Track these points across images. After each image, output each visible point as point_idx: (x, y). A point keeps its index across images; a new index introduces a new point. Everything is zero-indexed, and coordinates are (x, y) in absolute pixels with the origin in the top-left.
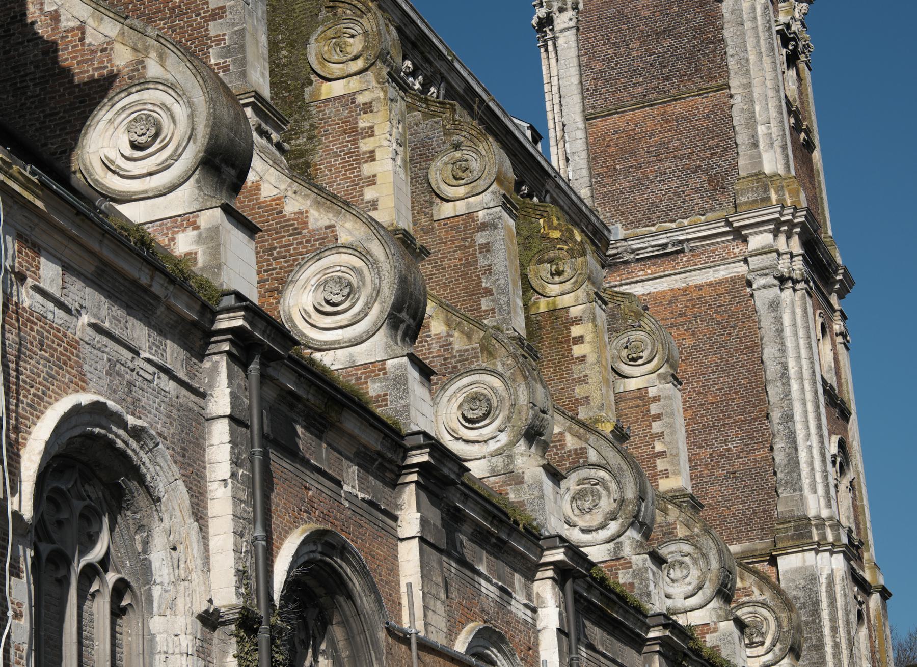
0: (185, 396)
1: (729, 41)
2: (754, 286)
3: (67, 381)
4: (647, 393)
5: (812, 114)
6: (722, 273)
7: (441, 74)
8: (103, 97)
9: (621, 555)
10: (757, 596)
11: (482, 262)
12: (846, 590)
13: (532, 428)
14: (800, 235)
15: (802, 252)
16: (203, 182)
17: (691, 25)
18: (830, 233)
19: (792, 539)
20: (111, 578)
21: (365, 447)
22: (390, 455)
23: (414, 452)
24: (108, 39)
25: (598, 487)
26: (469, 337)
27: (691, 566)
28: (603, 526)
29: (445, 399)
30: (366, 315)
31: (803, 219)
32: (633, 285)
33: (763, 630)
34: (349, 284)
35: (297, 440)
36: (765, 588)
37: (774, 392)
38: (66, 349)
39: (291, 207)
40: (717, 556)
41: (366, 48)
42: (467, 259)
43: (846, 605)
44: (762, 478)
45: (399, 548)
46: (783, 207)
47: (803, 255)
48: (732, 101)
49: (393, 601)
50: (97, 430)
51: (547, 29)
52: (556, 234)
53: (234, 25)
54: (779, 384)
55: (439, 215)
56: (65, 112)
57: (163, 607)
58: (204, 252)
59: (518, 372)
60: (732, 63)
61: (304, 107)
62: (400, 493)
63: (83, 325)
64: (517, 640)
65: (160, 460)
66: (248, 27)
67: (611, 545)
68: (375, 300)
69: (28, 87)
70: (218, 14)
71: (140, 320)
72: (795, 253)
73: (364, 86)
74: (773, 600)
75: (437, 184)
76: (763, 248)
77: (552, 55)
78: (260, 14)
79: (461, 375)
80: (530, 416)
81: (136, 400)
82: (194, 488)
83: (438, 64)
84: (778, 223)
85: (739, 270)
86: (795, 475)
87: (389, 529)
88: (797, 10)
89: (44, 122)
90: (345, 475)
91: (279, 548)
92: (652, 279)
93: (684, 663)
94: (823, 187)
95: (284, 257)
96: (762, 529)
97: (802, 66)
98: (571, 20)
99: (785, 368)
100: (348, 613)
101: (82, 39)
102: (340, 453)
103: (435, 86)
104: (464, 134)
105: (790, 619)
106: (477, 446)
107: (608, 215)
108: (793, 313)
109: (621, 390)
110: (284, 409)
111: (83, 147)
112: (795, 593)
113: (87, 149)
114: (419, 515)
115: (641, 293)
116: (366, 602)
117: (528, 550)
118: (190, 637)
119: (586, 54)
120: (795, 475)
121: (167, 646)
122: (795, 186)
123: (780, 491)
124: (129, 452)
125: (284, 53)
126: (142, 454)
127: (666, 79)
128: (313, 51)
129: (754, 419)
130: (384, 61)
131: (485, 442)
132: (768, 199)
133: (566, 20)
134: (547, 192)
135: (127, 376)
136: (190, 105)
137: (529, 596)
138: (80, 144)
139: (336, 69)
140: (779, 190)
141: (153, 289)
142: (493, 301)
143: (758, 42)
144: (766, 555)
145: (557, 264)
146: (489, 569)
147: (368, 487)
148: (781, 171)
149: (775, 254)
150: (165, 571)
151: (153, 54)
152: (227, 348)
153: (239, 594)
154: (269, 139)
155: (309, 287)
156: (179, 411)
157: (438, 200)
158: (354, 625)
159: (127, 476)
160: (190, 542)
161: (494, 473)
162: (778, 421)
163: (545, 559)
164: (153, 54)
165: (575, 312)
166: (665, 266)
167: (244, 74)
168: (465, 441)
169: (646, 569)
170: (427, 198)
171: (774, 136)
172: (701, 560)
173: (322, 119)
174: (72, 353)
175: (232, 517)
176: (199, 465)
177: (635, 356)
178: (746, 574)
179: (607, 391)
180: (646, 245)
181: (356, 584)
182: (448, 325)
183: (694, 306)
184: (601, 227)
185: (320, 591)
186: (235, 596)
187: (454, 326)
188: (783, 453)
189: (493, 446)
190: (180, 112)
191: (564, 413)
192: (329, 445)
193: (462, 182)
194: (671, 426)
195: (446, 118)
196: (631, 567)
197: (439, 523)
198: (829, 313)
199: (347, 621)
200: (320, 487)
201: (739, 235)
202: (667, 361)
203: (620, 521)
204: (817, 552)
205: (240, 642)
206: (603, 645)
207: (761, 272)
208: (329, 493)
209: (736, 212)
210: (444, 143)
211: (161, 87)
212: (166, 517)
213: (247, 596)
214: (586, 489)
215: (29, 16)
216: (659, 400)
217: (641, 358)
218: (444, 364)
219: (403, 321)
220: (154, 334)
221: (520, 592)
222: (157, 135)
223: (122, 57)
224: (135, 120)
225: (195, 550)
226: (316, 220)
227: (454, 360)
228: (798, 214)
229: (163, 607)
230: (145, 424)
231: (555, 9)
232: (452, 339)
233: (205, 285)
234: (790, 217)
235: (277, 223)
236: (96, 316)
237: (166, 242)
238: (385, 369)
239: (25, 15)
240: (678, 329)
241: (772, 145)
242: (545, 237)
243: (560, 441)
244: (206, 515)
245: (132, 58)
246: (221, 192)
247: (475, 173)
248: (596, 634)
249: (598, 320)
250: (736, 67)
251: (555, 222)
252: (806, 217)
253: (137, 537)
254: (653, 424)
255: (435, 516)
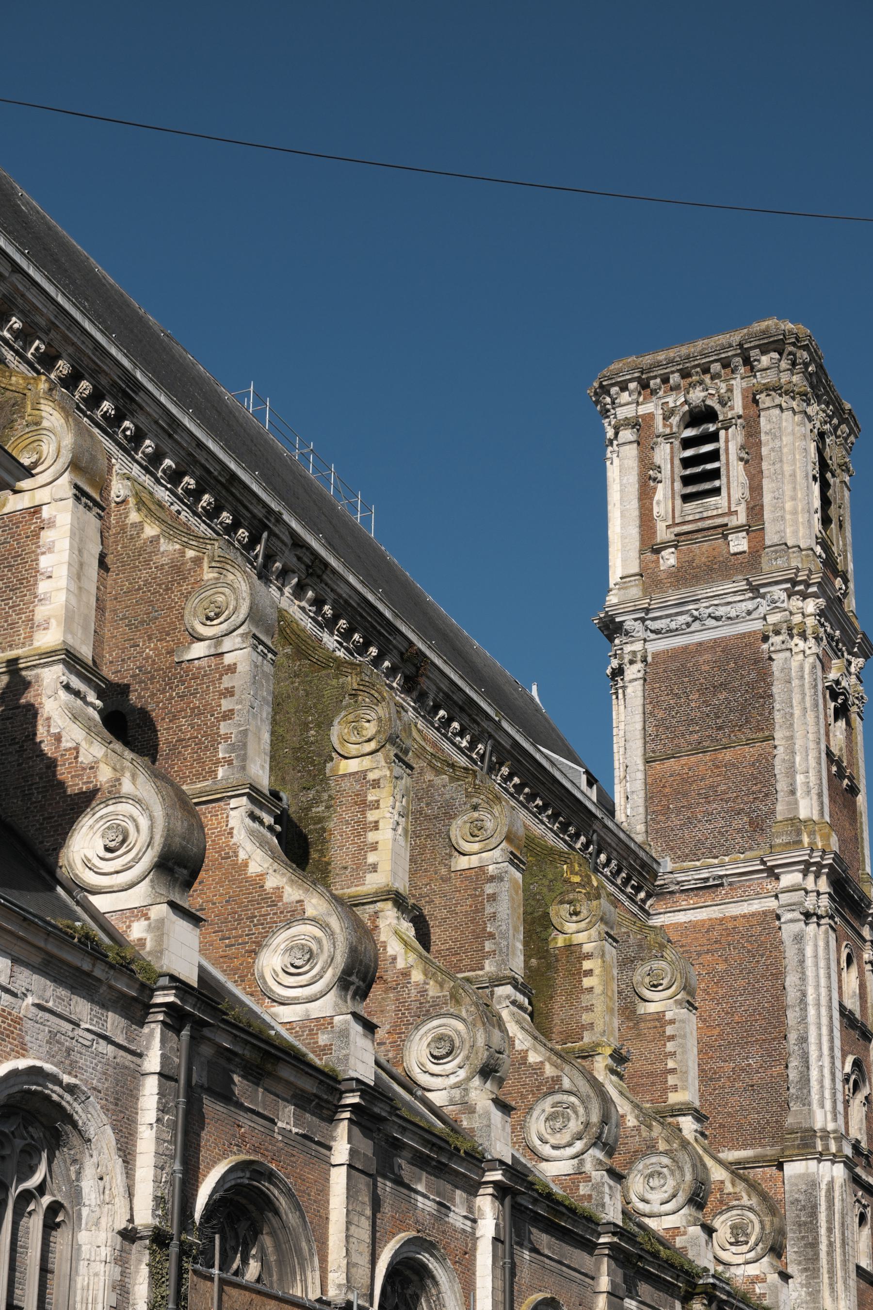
0: (122, 1056)
1: (776, 697)
2: (783, 920)
3: (8, 1050)
4: (664, 1016)
5: (860, 761)
6: (755, 906)
7: (488, 733)
8: (87, 807)
9: (583, 1170)
10: (745, 1201)
11: (489, 910)
12: (844, 1196)
13: (487, 1066)
14: (828, 875)
15: (828, 890)
16: (156, 881)
17: (745, 680)
18: (868, 869)
19: (798, 1148)
20: (46, 1200)
21: (302, 1090)
22: (326, 1097)
23: (348, 1095)
24: (95, 759)
25: (568, 1110)
26: (441, 986)
27: (668, 1176)
28: (570, 1145)
29: (418, 1037)
30: (321, 977)
31: (831, 861)
32: (677, 913)
33: (748, 1231)
34: (310, 951)
35: (233, 1086)
36: (753, 1194)
37: (793, 1016)
38: (9, 1025)
39: (271, 883)
40: (691, 1170)
41: (378, 732)
42: (476, 906)
43: (843, 1209)
44: (776, 1092)
45: (331, 1173)
46: (812, 850)
47: (829, 894)
48: (775, 752)
49: (320, 1216)
50: (34, 1088)
51: (618, 679)
52: (576, 879)
53: (240, 725)
54: (797, 1009)
55: (456, 866)
56: (59, 816)
57: (90, 1224)
58: (152, 940)
59: (478, 1018)
60: (778, 716)
61: (325, 780)
62: (336, 1127)
63: (27, 1005)
64: (452, 1246)
65: (90, 1109)
66: (252, 728)
67: (576, 1161)
68: (330, 966)
69: (33, 794)
70: (228, 715)
71: (84, 998)
72: (821, 891)
73: (374, 765)
74: (759, 1205)
75: (456, 839)
76: (792, 886)
77: (621, 702)
78: (264, 715)
79: (432, 1018)
80: (485, 1056)
81: (73, 1063)
82: (124, 1130)
83: (485, 724)
84: (808, 864)
85: (771, 904)
86: (805, 1091)
87: (322, 1157)
88: (853, 665)
89: (42, 824)
90: (280, 1113)
91: (205, 1176)
92: (693, 909)
93: (639, 1263)
94: (866, 828)
95: (262, 924)
96: (773, 1138)
97: (854, 717)
98: (639, 671)
99: (804, 995)
100: (276, 1226)
101: (76, 757)
102: (278, 1096)
103: (482, 743)
104: (482, 797)
105: (772, 1223)
106: (440, 1078)
107: (660, 849)
108: (816, 946)
109: (642, 1012)
110: (223, 1062)
111: (69, 847)
112: (797, 1196)
113: (72, 848)
114: (349, 1146)
115: (683, 921)
116: (292, 1218)
117: (470, 1171)
118: (109, 1249)
119: (651, 703)
120: (805, 1091)
121: (90, 1254)
122: (827, 831)
123: (791, 1105)
124: (64, 1103)
125: (312, 732)
126: (75, 1105)
127: (720, 728)
128: (336, 732)
129: (774, 1039)
130: (394, 743)
131: (447, 1076)
132: (800, 842)
133: (635, 671)
134: (594, 831)
135: (67, 1044)
136: (151, 818)
137: (470, 1209)
138: (66, 844)
139: (353, 749)
140: (812, 834)
141: (94, 974)
142: (494, 944)
143: (803, 698)
144: (775, 1160)
145: (575, 906)
146: (428, 1187)
147: (304, 1123)
148: (816, 817)
149: (803, 892)
150: (93, 1196)
151: (128, 774)
152: (162, 1019)
153: (154, 1215)
154: (261, 822)
155: (279, 951)
156: (115, 1068)
157: (456, 854)
158: (280, 1236)
159: (63, 1122)
160: (115, 1174)
161: (452, 1103)
162: (793, 1042)
163: (485, 1179)
164: (128, 774)
165: (587, 948)
166: (706, 898)
167: (243, 768)
168: (430, 1074)
169: (603, 1184)
170: (447, 851)
171: (811, 784)
172: (677, 1172)
173: (338, 792)
174: (15, 1028)
175: (153, 1154)
176: (131, 1112)
177: (655, 983)
178: (738, 1181)
179: (611, 1019)
180: (690, 878)
181: (283, 1203)
182: (426, 975)
183: (728, 935)
184: (649, 861)
185: (251, 1208)
186: (150, 1217)
187: (430, 976)
188: (796, 1071)
189: (453, 1080)
190: (144, 823)
191: (545, 1045)
192: (265, 1089)
193: (477, 839)
194: (682, 1046)
195: (468, 783)
196: (590, 1181)
197: (370, 1153)
198: (860, 943)
199: (275, 1232)
200: (252, 1125)
201: (772, 873)
202: (684, 989)
203: (585, 1141)
204: (819, 1161)
205: (153, 1253)
206: (549, 1248)
207: (789, 908)
208: (262, 1130)
209: (771, 853)
210: (465, 804)
211: (131, 802)
212: (95, 1153)
213: (164, 1217)
214: (557, 1112)
215: (38, 736)
216: (674, 1023)
217: (661, 984)
218: (420, 1008)
219: (353, 983)
220: (96, 1008)
221: (460, 1206)
222: (124, 841)
223: (105, 775)
224: (108, 828)
225: (119, 1181)
226: (290, 895)
227: (427, 1005)
228: (827, 857)
229: (90, 1224)
230: (78, 1082)
231: (626, 661)
232: (427, 987)
233: (147, 968)
234: (818, 859)
235: (259, 896)
236: (40, 997)
237: (125, 929)
238: (332, 1023)
239: (35, 734)
240: (713, 955)
241: (809, 792)
242: (567, 881)
243: (540, 1069)
244: (135, 1151)
245: (112, 776)
246: (174, 888)
247: (489, 831)
248: (543, 1240)
249: (607, 956)
250: (781, 721)
251: (577, 868)
252: (833, 859)
253: (72, 1168)
254: (668, 1044)
255: (367, 1147)
